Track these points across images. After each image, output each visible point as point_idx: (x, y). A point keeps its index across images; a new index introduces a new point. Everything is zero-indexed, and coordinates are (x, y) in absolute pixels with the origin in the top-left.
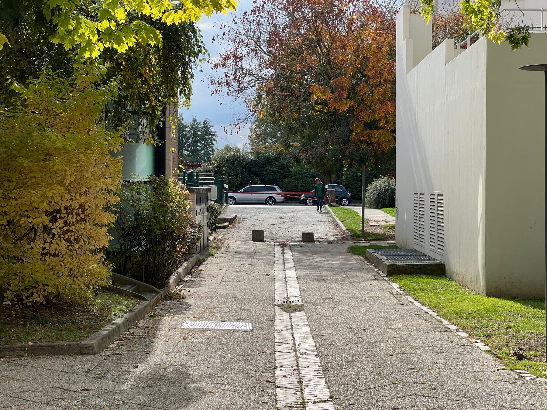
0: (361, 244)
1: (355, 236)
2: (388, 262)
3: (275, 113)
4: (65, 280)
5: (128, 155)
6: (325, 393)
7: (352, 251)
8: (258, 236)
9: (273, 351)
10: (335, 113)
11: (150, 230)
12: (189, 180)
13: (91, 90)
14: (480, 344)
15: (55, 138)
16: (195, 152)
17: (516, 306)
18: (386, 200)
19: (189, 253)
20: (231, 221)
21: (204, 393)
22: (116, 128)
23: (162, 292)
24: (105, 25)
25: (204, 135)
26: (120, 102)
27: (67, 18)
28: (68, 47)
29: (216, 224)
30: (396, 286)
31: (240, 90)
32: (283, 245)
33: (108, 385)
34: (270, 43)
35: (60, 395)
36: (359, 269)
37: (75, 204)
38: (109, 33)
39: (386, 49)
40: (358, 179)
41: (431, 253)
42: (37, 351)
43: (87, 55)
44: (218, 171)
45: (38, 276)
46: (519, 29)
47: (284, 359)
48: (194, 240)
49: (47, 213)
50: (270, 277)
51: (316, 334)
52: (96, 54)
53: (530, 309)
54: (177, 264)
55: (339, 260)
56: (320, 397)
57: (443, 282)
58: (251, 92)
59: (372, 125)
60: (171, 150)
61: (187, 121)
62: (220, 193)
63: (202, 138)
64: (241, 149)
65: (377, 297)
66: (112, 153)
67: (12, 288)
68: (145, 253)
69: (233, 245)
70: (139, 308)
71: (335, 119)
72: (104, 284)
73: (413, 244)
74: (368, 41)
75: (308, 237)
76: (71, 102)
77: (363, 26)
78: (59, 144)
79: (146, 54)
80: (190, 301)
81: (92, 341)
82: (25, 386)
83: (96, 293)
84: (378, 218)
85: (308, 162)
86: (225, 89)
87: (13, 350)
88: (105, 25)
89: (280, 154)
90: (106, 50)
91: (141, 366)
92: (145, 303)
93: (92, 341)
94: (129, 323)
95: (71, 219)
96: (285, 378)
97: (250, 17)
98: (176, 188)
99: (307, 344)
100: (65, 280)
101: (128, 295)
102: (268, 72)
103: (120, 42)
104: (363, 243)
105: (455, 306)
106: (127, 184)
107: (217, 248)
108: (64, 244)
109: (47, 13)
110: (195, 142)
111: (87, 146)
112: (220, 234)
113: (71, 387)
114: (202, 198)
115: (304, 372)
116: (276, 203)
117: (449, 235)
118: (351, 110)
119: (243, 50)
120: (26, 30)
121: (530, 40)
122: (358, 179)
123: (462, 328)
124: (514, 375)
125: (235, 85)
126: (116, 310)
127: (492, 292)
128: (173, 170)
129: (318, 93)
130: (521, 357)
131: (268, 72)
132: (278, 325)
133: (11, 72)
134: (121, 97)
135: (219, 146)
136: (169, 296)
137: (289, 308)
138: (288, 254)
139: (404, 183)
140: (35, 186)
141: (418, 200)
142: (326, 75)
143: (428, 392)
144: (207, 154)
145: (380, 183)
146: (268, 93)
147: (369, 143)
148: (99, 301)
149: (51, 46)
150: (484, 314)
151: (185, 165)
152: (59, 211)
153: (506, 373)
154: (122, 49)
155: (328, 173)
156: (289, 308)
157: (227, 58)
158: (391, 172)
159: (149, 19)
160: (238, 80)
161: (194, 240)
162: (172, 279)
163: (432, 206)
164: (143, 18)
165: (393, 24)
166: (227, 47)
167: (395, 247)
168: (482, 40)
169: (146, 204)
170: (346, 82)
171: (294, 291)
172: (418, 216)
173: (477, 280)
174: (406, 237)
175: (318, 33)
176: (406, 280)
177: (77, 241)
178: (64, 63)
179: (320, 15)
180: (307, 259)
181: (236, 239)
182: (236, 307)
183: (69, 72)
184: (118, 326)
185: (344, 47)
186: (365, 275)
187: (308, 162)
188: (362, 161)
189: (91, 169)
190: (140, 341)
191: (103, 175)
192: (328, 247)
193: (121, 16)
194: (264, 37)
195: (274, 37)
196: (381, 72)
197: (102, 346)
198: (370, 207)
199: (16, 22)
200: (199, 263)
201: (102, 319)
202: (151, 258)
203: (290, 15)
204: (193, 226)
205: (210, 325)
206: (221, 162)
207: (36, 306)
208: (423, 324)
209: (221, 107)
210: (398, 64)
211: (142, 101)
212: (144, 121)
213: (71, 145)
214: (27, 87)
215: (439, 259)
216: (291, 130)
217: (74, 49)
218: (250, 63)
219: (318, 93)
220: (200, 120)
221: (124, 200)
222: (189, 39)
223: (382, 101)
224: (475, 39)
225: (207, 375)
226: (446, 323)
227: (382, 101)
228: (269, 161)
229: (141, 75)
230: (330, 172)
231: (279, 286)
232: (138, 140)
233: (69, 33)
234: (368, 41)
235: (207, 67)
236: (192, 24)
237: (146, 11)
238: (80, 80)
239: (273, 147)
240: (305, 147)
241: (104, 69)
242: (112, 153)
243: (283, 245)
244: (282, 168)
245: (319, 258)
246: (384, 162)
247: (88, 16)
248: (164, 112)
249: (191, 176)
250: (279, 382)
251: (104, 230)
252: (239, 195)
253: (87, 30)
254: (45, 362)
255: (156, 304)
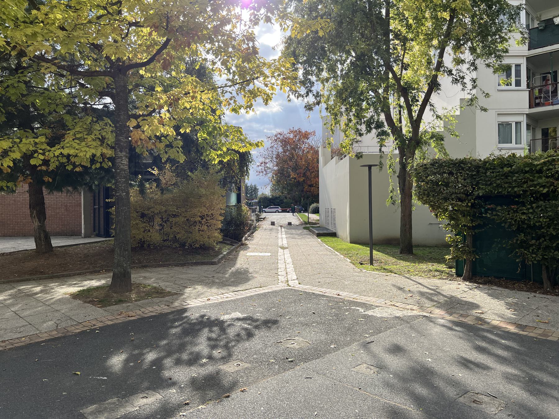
0: (308, 226)
1: (306, 223)
2: (317, 232)
3: (278, 182)
4: (206, 239)
5: (228, 197)
6: (295, 277)
7: (305, 228)
8: (273, 224)
9: (278, 263)
10: (298, 181)
11: (236, 222)
12: (249, 205)
13: (215, 174)
14: (348, 260)
15: (203, 191)
16: (252, 195)
17: (360, 247)
18: (316, 211)
19: (249, 229)
20: (264, 219)
21: (254, 277)
22: (224, 187)
23: (240, 243)
24: (219, 152)
25: (255, 190)
26: (225, 179)
27: (206, 150)
28: (207, 160)
29: (258, 220)
30: (319, 240)
31: (266, 174)
32: (281, 226)
33: (221, 275)
34: (276, 158)
35: (204, 279)
36: (307, 234)
37: (210, 213)
38: (221, 155)
39: (315, 160)
40: (307, 204)
41: (332, 229)
42: (197, 264)
43: (213, 163)
44: (259, 202)
45: (197, 238)
46: (359, 153)
47: (281, 265)
48: (251, 225)
49: (200, 217)
50: (277, 238)
51: (292, 257)
52: (216, 162)
53: (364, 247)
54: (245, 233)
55: (300, 231)
56: (293, 278)
57: (336, 239)
58: (270, 175)
59: (311, 186)
60: (243, 195)
61: (249, 185)
62: (260, 209)
63: (254, 191)
64: (286, 132)
65: (314, 243)
66: (222, 196)
67: (189, 242)
68: (234, 230)
69: (265, 227)
70: (232, 248)
71: (298, 184)
72: (220, 240)
73: (325, 225)
74: (309, 157)
75: (290, 224)
76: (208, 178)
77: (308, 152)
78: (204, 193)
79: (234, 162)
80: (250, 246)
81: (216, 260)
82: (193, 276)
83: (217, 244)
84: (313, 217)
85: (290, 198)
86: (261, 174)
87: (189, 263)
88: (219, 152)
89: (280, 196)
90: (220, 161)
91: (232, 269)
92: (234, 247)
93: (216, 260)
94: (229, 254)
95: (208, 219)
96: (281, 272)
97: (269, 150)
98: (245, 208)
99: (289, 260)
100: (206, 239)
101: (228, 244)
102: (276, 168)
103: (224, 158)
104: (308, 226)
105: (339, 247)
106: (227, 206)
107: (259, 228)
108: (206, 227)
109: (200, 149)
110: (252, 192)
111: (214, 194)
112: (260, 223)
113: (209, 276)
114: (254, 211)
115: (288, 270)
116: (279, 212)
117: (337, 222)
118: (304, 180)
119: (267, 161)
120: (193, 155)
121: (363, 157)
122: (307, 204)
123: (342, 254)
124: (359, 270)
125: (265, 172)
126: (224, 250)
127: (353, 241)
128: (244, 201)
129: (293, 175)
130: (361, 264)
131: (276, 168)
132: (279, 254)
133: (188, 169)
134: (225, 177)
135: (260, 193)
136: (243, 244)
137: (283, 248)
138: (283, 230)
139: (322, 205)
140: (196, 207)
141: (327, 211)
142: (295, 169)
143: (330, 276)
144: (256, 196)
145: (314, 205)
146: (276, 175)
147: (310, 192)
148: (218, 246)
149: (201, 160)
150: (349, 249)
151: (248, 200)
152: (204, 216)
153: (356, 269)
154: (225, 160)
155: (296, 202)
156: (283, 248)
157: (262, 163)
158: (318, 202)
159: (234, 150)
160: (266, 171)
161: (251, 225)
162: (244, 238)
163: (332, 213)
164: (232, 150)
165: (318, 152)
166: (262, 160)
167: (319, 227)
168: (347, 157)
169: (234, 213)
170: (302, 171)
171: (285, 243)
172: (327, 217)
173: (347, 238)
174: (323, 223)
175: (293, 155)
176: (323, 238)
177: (210, 226)
178: (206, 165)
179: (293, 148)
180: (290, 231)
181: (265, 224)
182: (265, 248)
183: (207, 168)
184: (225, 255)
185: (301, 159)
186: (309, 236)
187: (290, 198)
188: (308, 198)
189: (215, 201)
190: (232, 260)
191: (219, 203)
192: (297, 227)
193: (225, 149)
194: (274, 156)
195: (278, 156)
196: (314, 168)
197: (219, 262)
198: (311, 213)
199: (189, 152)
200: (253, 233)
201: (219, 252)
202: (236, 232)
203: (283, 149)
204: (250, 220)
205: (257, 254)
206: (261, 198)
207: (196, 248)
208: (329, 253)
209: (260, 179)
210: (319, 165)
211: (232, 178)
212: (233, 185)
213: (208, 193)
214: (193, 173)
215: (334, 231)
216: (284, 188)
217: (209, 161)
218: (270, 165)
219: (293, 175)
220: (253, 184)
221: (226, 212)
222: (248, 157)
223: (314, 177)
224: (345, 156)
225: (255, 271)
226: (336, 252)
227: (314, 177)
228: (276, 198)
229: (232, 169)
230: (297, 202)
231: (280, 240)
232: (231, 191)
233: (207, 155)
234: (309, 157)
235: (255, 166)
236: (249, 152)
237: (233, 148)
238: (211, 171)
239: (278, 193)
240: (288, 194)
241: (219, 167)
242: (222, 196)
243: (281, 226)
244: (281, 200)
245: (293, 231)
246: (316, 198)
247: (214, 150)
248: (240, 182)
249: (250, 203)
250: (279, 274)
251: (220, 222)
252: (266, 210)
253: (213, 154)
254: (199, 267)
255: (238, 247)
